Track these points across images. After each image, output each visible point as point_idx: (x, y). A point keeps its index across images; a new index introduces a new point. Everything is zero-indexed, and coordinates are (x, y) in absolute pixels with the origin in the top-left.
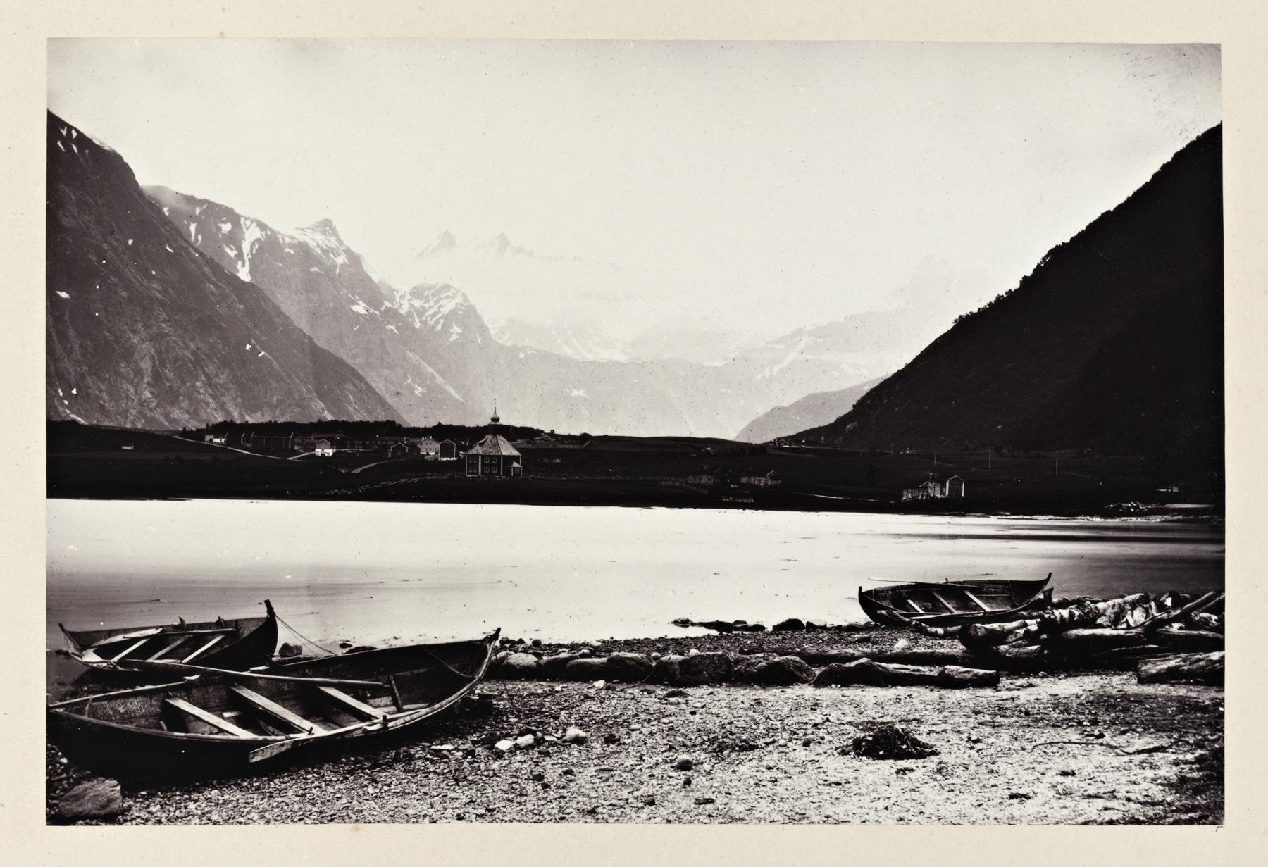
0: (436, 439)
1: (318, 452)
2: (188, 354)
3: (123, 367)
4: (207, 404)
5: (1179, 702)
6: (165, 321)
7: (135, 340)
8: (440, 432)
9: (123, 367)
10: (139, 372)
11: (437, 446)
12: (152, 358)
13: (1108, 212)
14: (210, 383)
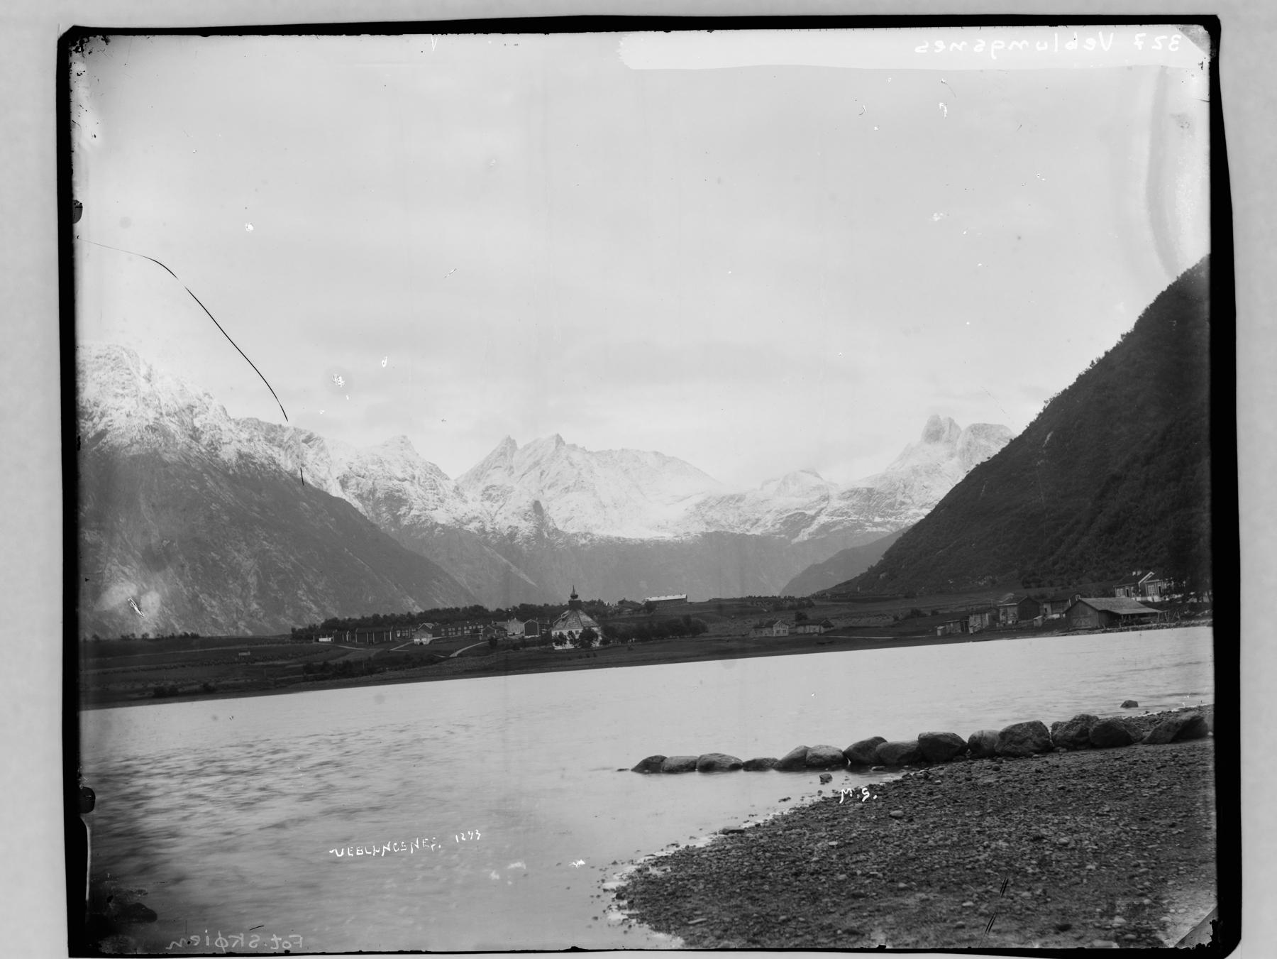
0: (522, 619)
1: (417, 640)
2: (289, 566)
3: (232, 585)
4: (310, 609)
5: (832, 822)
6: (265, 539)
7: (239, 558)
8: (524, 612)
9: (232, 585)
10: (245, 586)
11: (522, 626)
12: (257, 573)
13: (1163, 293)
14: (311, 590)
